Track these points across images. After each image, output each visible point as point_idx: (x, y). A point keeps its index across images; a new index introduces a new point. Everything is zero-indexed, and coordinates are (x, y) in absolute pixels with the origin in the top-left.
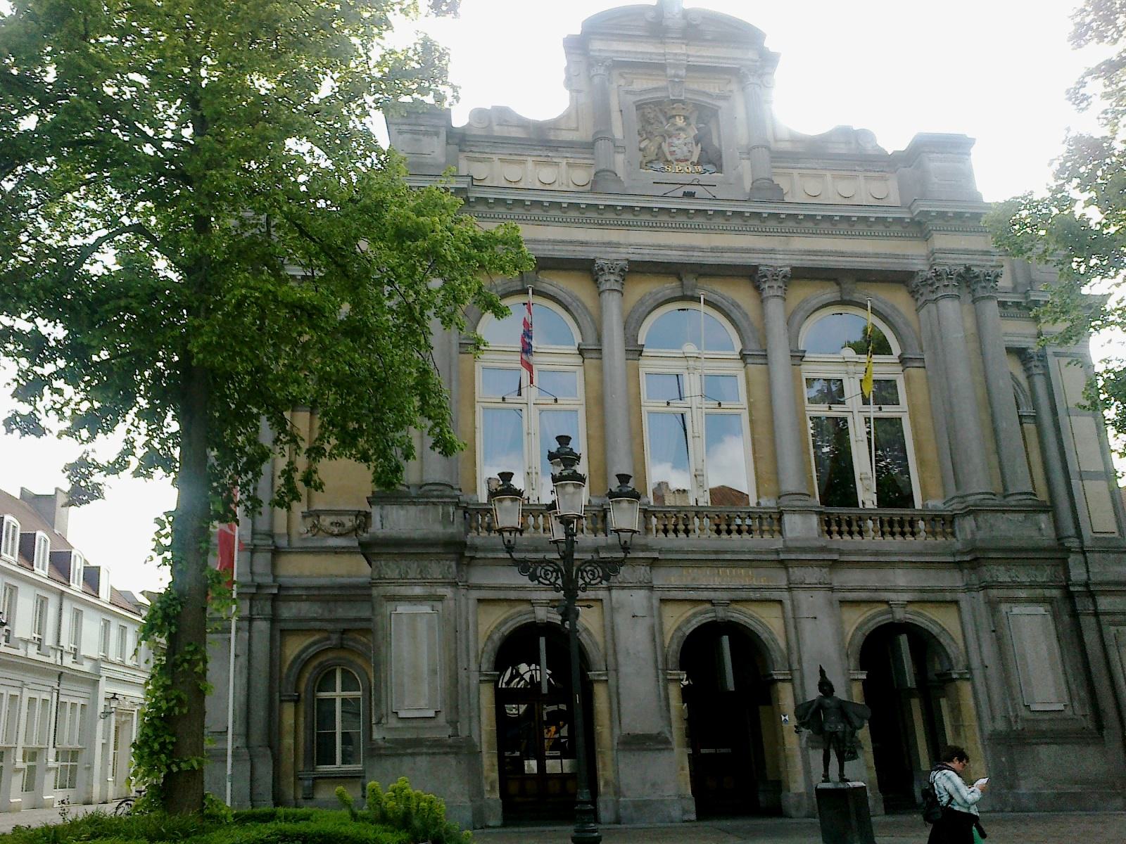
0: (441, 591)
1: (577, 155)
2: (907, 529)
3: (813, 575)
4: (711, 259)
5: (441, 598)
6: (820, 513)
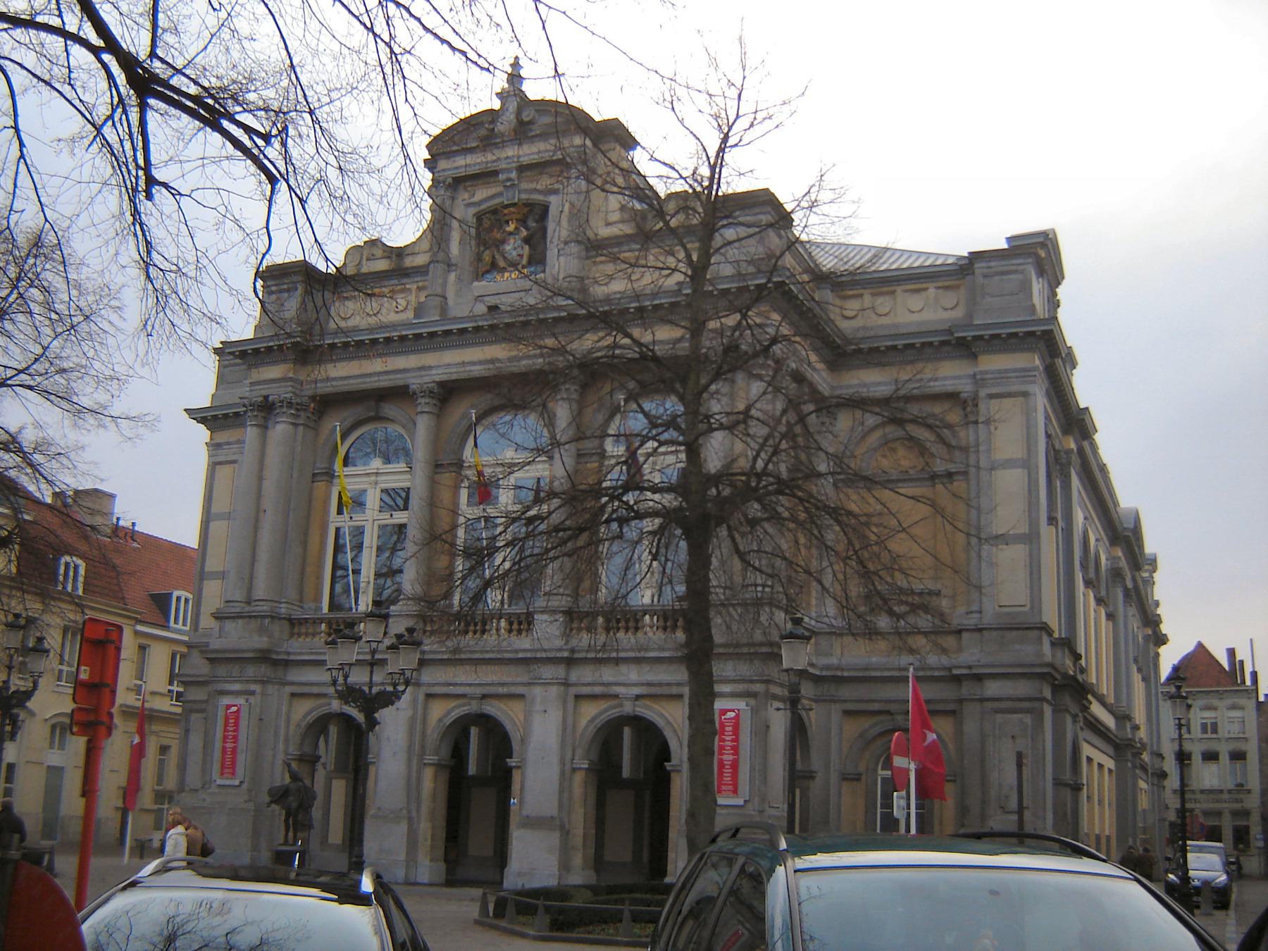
0: (253, 687)
3: (548, 672)
5: (253, 693)
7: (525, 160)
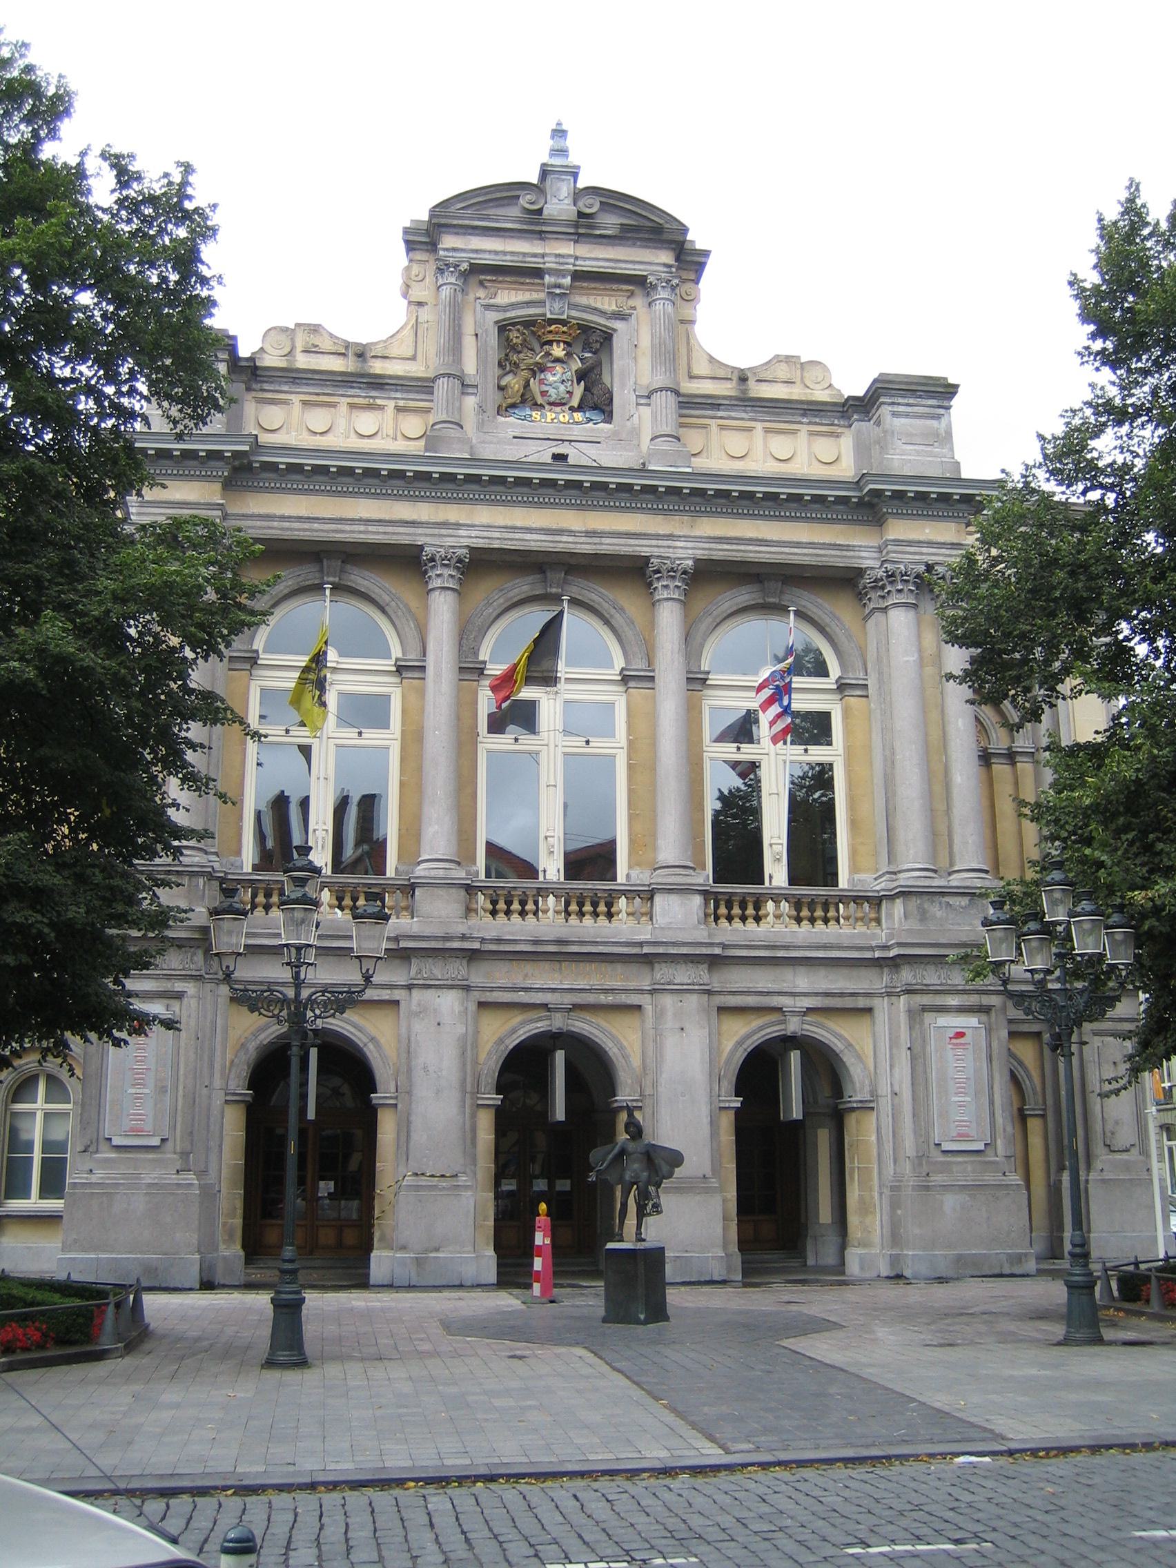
0: (179, 986)
1: (412, 396)
2: (750, 911)
3: (683, 975)
4: (586, 547)
6: (705, 894)
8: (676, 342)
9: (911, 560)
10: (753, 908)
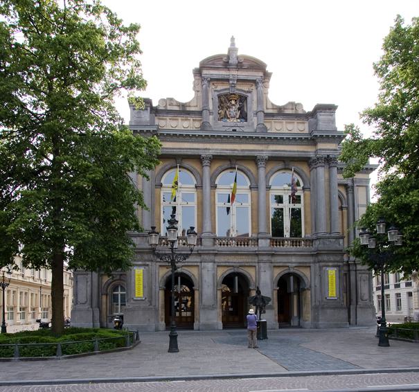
0: (147, 263)
3: (265, 258)
5: (148, 265)
7: (242, 77)
8: (261, 100)
9: (324, 154)
10: (282, 243)
